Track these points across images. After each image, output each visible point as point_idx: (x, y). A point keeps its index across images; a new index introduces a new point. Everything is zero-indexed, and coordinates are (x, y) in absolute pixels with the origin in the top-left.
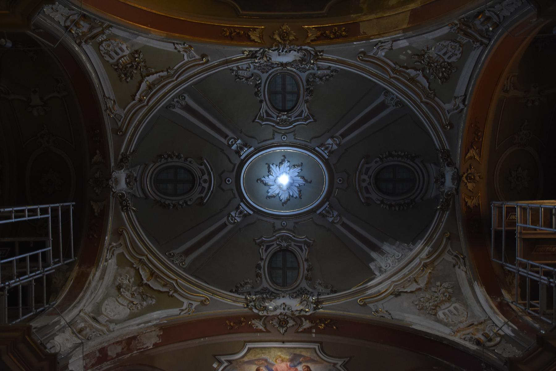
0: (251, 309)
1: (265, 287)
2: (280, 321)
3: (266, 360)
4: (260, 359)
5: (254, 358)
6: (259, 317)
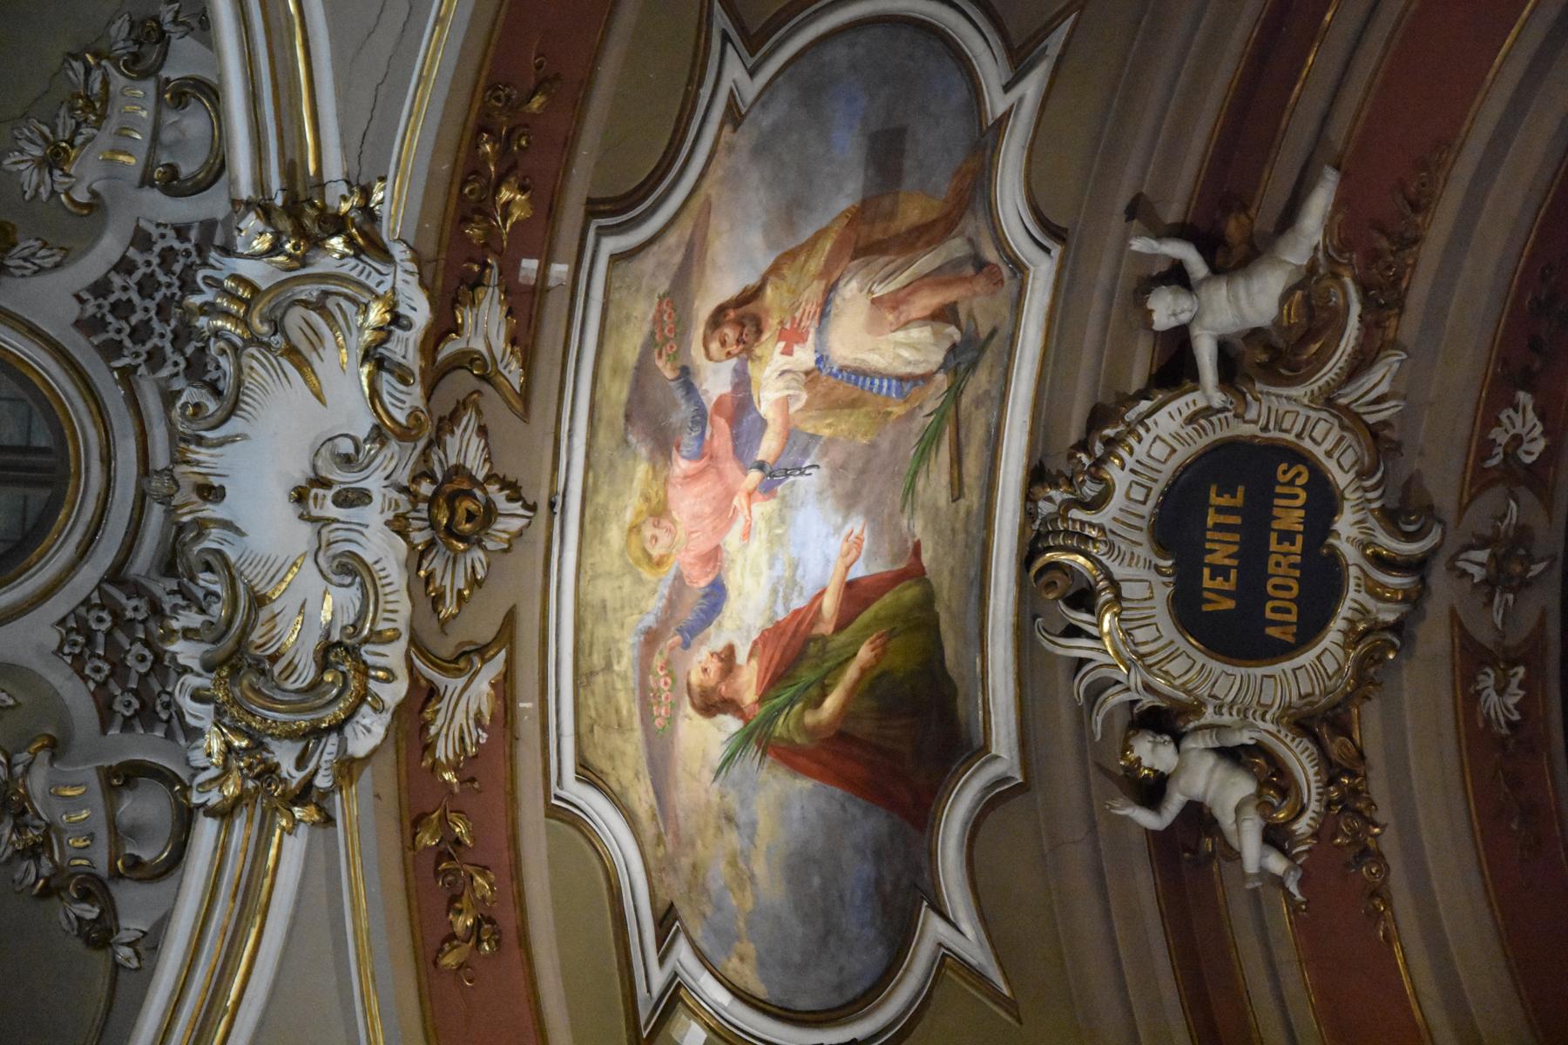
0: (348, 767)
1: (53, 638)
2: (451, 532)
3: (651, 639)
4: (643, 686)
5: (638, 734)
6: (424, 695)
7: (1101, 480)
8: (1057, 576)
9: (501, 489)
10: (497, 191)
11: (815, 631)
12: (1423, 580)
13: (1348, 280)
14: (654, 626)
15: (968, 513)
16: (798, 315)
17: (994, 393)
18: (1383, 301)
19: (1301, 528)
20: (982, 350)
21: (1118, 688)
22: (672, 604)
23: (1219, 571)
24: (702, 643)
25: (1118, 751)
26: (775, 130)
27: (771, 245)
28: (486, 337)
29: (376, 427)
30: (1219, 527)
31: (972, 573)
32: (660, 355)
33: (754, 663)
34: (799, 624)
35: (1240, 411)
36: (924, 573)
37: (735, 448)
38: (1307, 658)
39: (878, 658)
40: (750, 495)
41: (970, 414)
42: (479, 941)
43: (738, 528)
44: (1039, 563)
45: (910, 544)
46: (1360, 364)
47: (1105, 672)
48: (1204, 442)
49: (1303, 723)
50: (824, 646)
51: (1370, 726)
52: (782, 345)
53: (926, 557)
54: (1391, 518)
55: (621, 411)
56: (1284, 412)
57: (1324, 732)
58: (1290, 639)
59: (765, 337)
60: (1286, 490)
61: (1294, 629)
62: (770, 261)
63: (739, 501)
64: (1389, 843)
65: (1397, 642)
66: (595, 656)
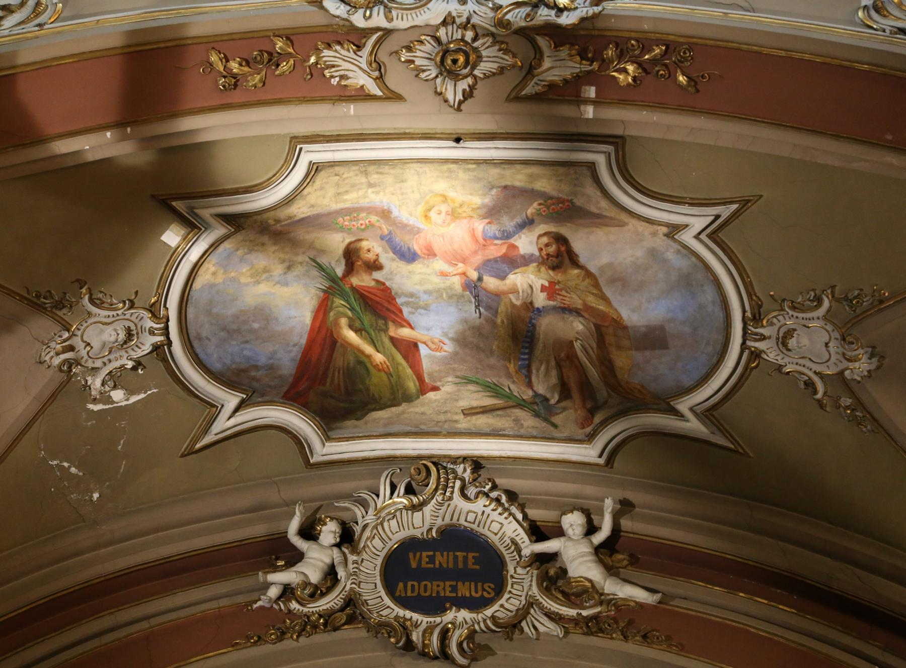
4: (360, 210)
7: (476, 497)
8: (424, 474)
9: (469, 86)
10: (633, 62)
11: (390, 324)
12: (436, 658)
13: (598, 609)
14: (392, 216)
15: (456, 421)
16: (563, 293)
17: (522, 431)
18: (593, 626)
19: (460, 595)
20: (546, 420)
21: (364, 513)
22: (404, 226)
23: (432, 559)
24: (384, 248)
25: (329, 514)
26: (665, 261)
27: (602, 269)
28: (552, 68)
29: (501, 7)
30: (456, 558)
31: (423, 427)
32: (540, 204)
33: (373, 284)
34: (394, 312)
35: (521, 564)
36: (423, 395)
37: (489, 261)
38: (388, 601)
39: (376, 367)
40: (464, 274)
41: (510, 416)
42: (225, 77)
43: (446, 268)
44: (433, 469)
45: (438, 384)
46: (550, 615)
47: (372, 504)
48: (503, 550)
49: (351, 601)
50: (382, 330)
51: (349, 633)
52: (547, 284)
53: (431, 395)
54: (472, 634)
55: (509, 183)
56: (522, 584)
57: (348, 611)
58: (397, 594)
59: (551, 272)
60: (480, 587)
61: (403, 595)
62: (593, 270)
63: (461, 267)
64: (289, 644)
65: (400, 644)
66: (376, 176)
